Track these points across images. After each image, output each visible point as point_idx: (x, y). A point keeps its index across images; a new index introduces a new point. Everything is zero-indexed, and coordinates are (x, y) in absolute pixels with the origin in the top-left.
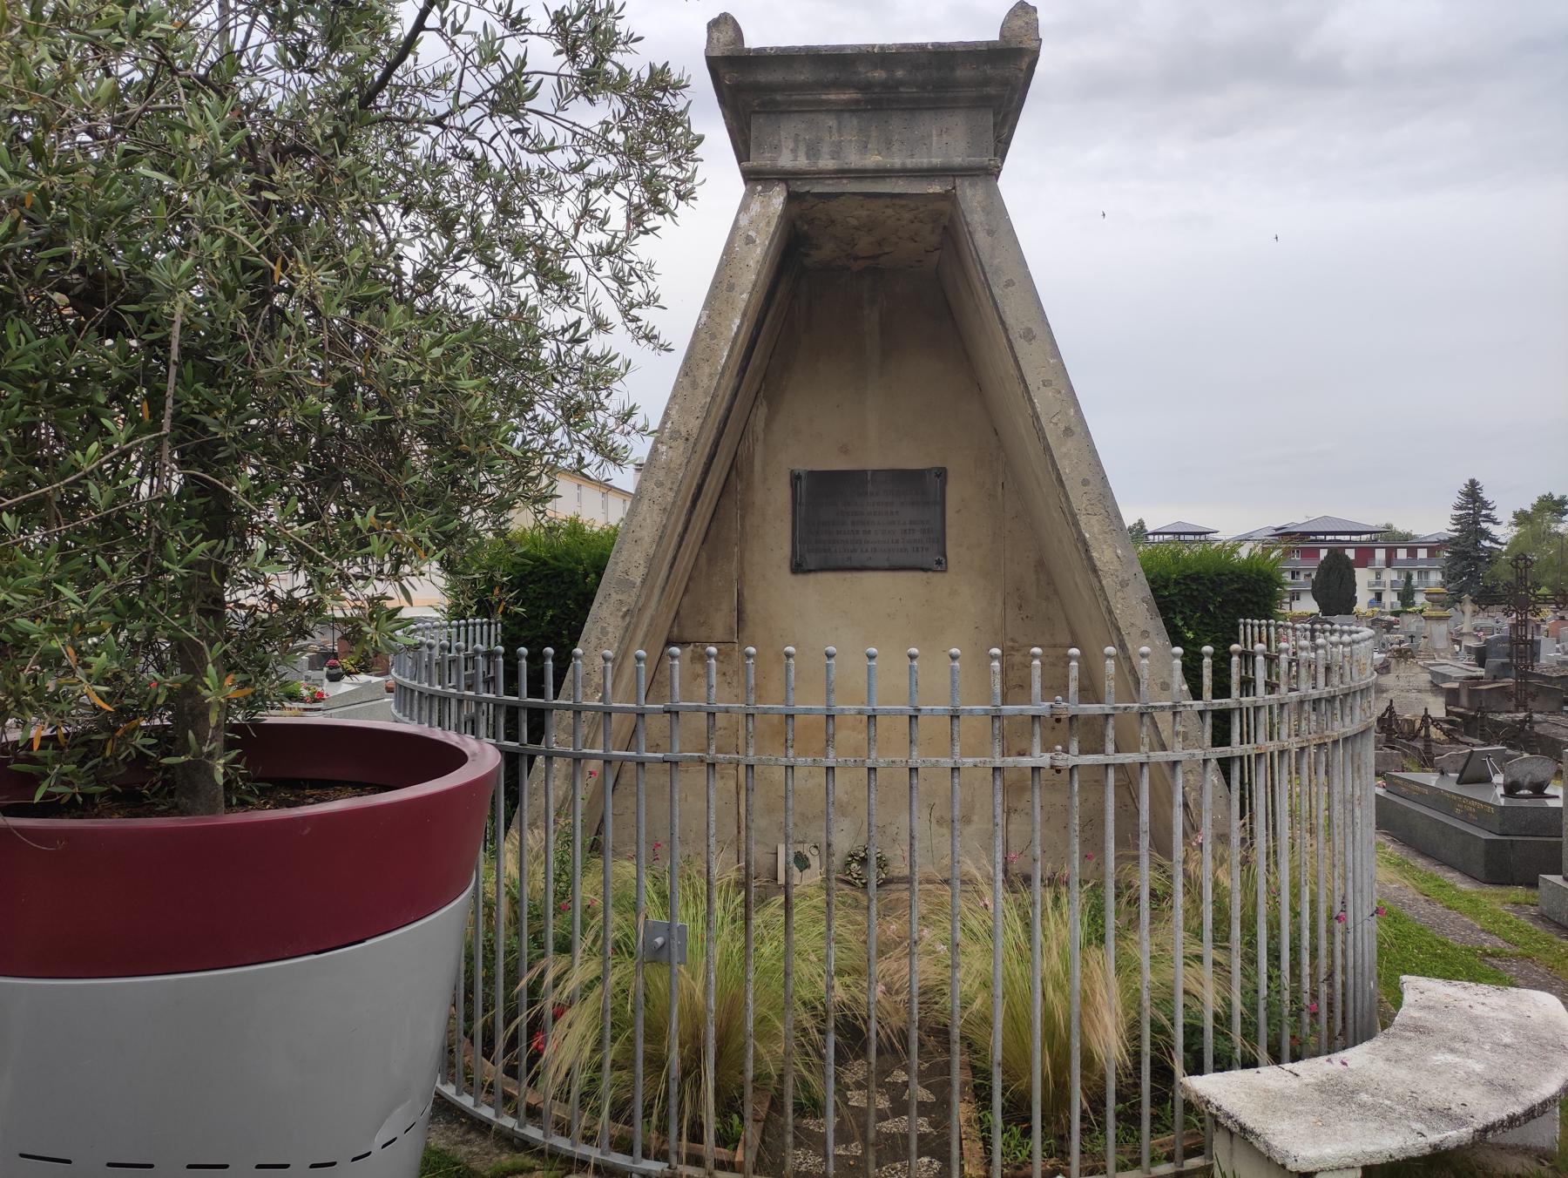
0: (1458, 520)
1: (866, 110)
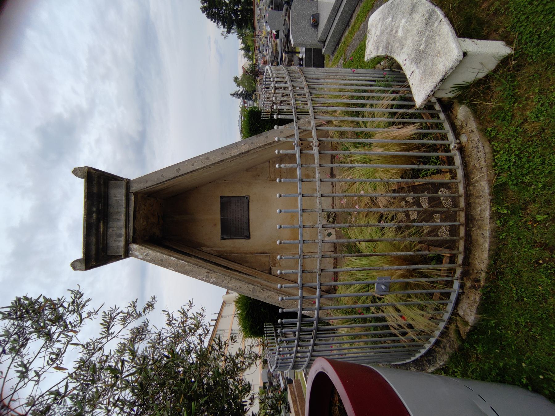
0: (238, 98)
1: (107, 220)
